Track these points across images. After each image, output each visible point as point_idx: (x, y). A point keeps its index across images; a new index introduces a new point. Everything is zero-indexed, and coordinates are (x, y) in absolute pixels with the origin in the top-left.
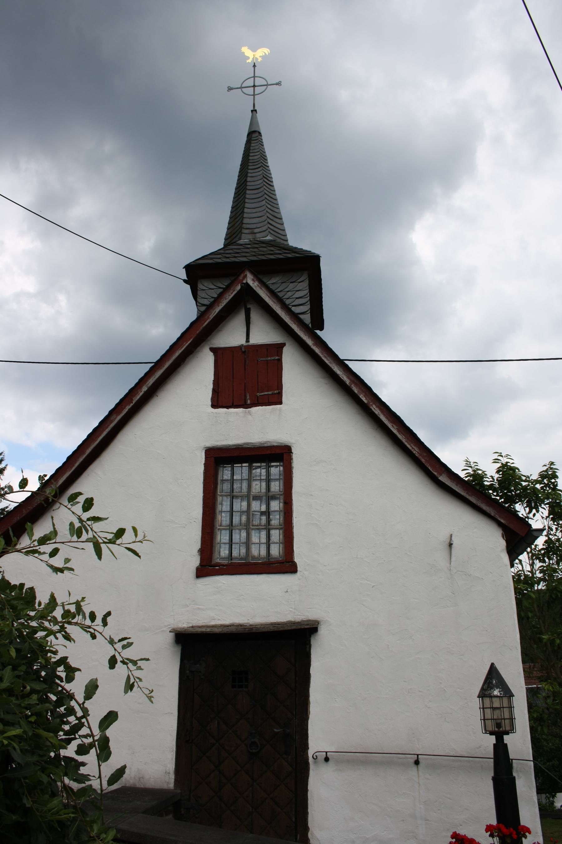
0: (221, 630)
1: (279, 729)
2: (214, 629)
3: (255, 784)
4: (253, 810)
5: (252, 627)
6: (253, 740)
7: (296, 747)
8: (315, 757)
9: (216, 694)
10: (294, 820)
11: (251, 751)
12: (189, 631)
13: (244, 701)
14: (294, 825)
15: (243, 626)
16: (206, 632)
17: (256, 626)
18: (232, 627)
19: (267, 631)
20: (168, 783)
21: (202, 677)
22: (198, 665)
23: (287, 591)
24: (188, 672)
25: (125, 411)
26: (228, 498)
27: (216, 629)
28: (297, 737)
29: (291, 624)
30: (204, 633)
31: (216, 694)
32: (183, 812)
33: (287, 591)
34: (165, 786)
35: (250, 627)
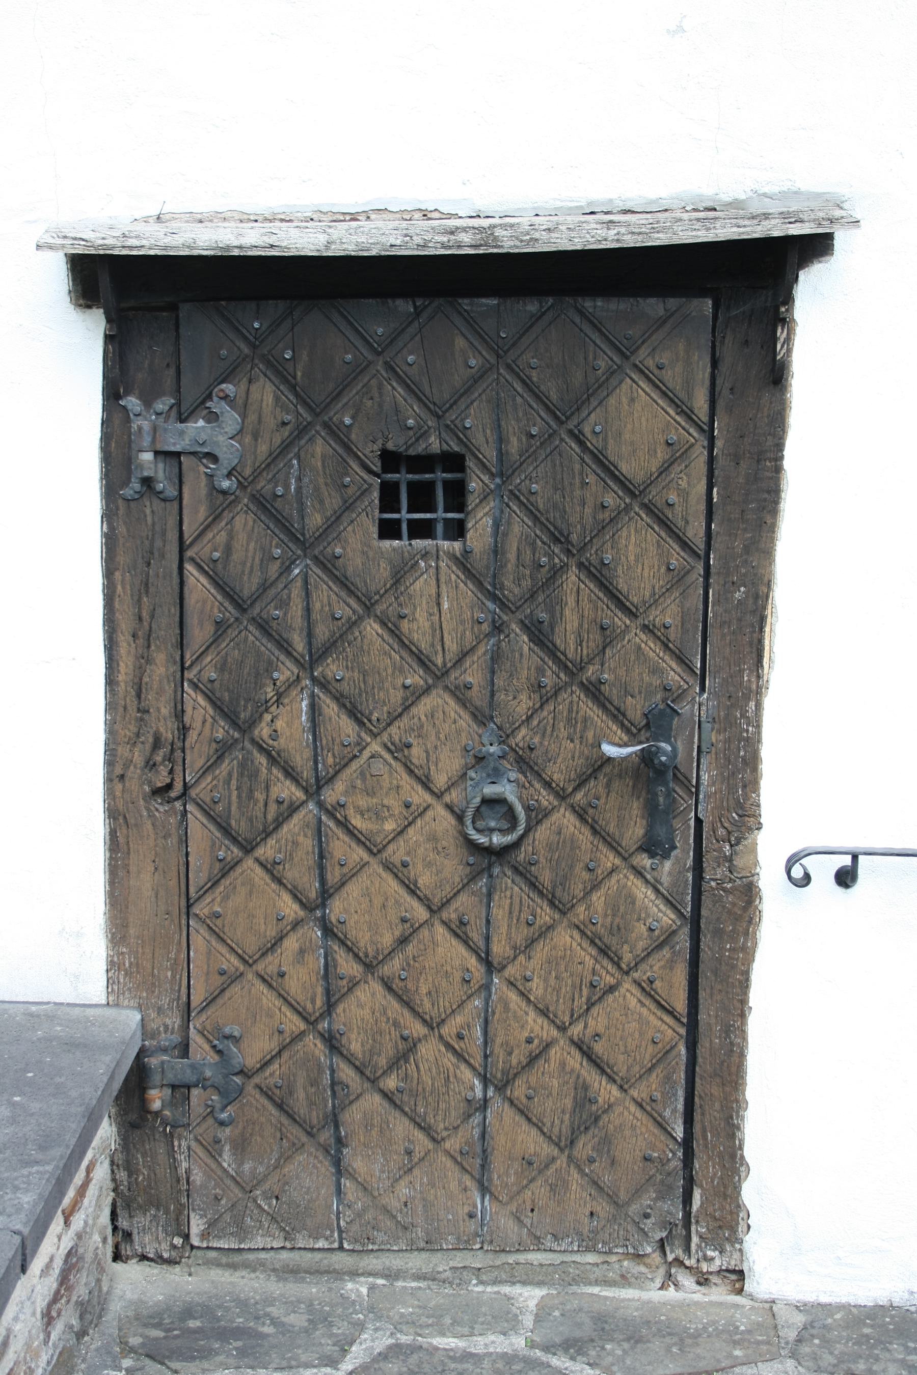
0: (322, 239)
1: (626, 745)
2: (282, 235)
3: (496, 980)
4: (490, 1093)
5: (485, 223)
6: (490, 790)
7: (699, 822)
8: (797, 872)
9: (297, 571)
10: (679, 1133)
11: (482, 840)
12: (144, 242)
13: (446, 606)
14: (680, 1154)
15: (436, 215)
16: (240, 247)
17: (508, 220)
18: (380, 224)
19: (579, 248)
20: (77, 977)
21: (226, 484)
22: (201, 423)
23: (680, 29)
24: (147, 456)
25: (492, 435)
26: (121, 1290)
27: (294, 233)
28: (705, 777)
29: (695, 210)
30: (236, 253)
31: (297, 571)
32: (156, 1105)
33: (680, 29)
34: (64, 993)
35: (476, 222)
